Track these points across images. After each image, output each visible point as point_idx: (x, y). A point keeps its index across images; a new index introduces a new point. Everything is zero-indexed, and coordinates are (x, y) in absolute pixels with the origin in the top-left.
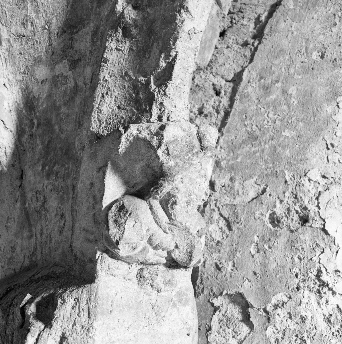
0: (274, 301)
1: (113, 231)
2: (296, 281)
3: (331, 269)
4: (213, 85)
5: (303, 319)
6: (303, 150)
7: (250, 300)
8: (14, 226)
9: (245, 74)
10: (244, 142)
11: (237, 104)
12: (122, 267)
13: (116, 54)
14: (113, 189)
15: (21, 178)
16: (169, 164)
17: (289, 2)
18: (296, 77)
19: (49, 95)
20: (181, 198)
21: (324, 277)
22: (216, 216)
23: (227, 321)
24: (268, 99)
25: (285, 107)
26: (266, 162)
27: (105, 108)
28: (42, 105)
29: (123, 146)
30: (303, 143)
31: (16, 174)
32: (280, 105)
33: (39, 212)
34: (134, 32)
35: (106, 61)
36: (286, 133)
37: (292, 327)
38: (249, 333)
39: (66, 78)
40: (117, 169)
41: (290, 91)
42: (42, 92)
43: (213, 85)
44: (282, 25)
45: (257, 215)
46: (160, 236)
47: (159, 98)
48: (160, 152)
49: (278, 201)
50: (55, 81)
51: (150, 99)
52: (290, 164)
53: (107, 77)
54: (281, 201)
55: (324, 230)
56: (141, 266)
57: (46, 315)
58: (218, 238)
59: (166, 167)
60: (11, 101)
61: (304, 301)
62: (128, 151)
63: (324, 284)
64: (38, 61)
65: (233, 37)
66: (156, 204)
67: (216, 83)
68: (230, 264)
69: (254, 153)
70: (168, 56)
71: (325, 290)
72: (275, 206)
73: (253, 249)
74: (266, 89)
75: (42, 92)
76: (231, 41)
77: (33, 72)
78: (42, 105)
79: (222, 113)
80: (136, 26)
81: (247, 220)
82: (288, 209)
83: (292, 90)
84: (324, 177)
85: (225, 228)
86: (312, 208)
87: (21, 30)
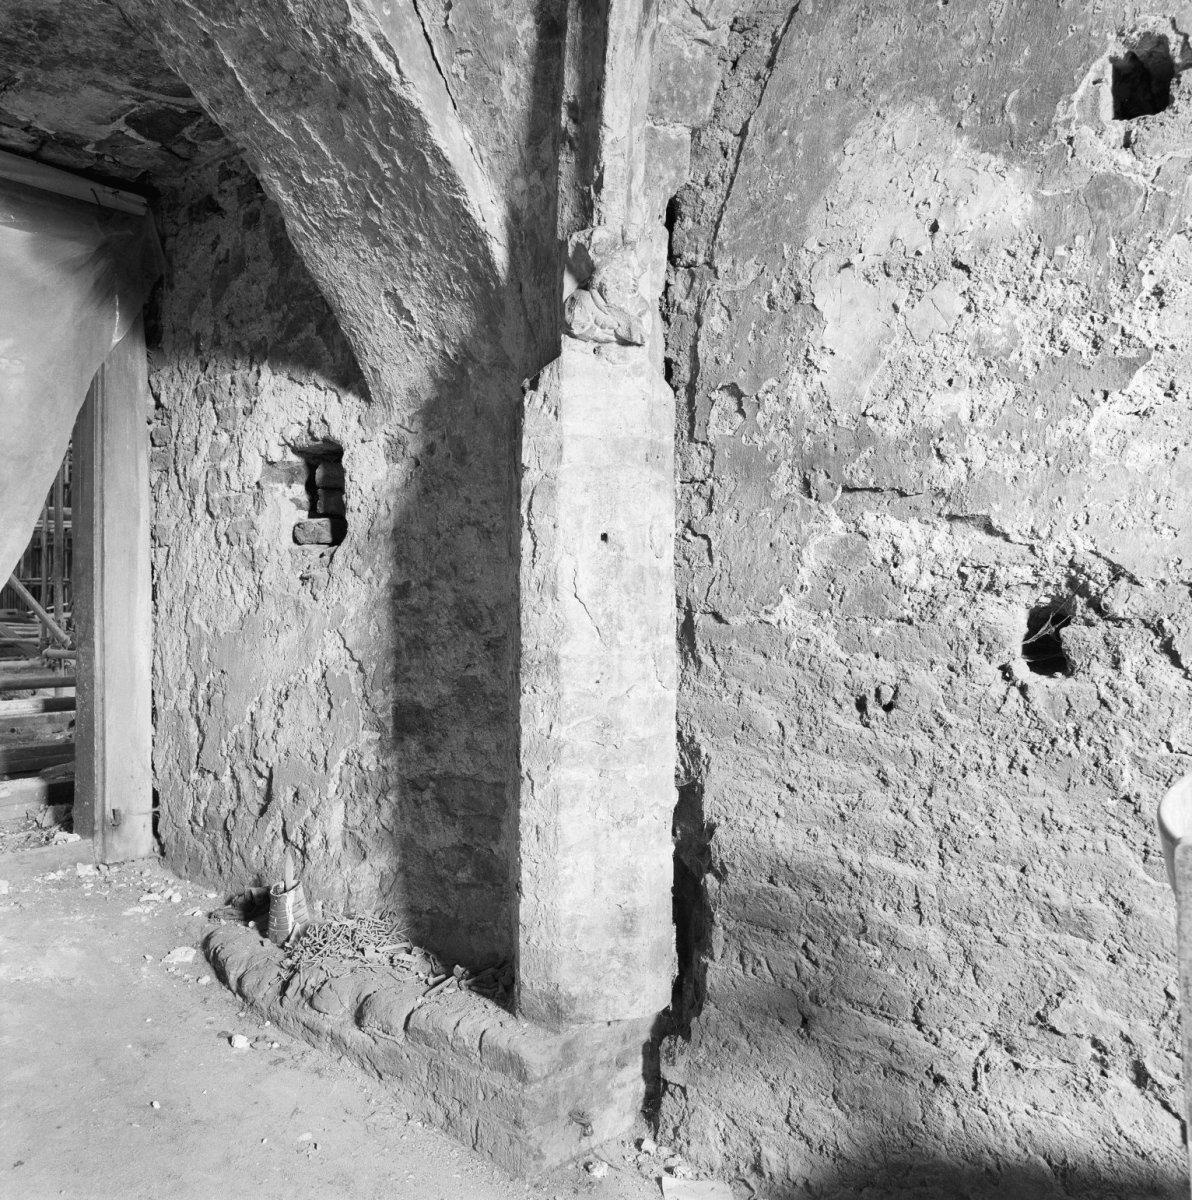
0: (765, 387)
1: (568, 316)
2: (787, 364)
3: (818, 346)
4: (721, 143)
5: (789, 400)
6: (803, 217)
7: (743, 389)
8: (522, 340)
9: (751, 124)
10: (746, 215)
11: (741, 164)
12: (578, 344)
13: (567, 163)
14: (569, 285)
15: (521, 290)
16: (597, 260)
17: (808, 8)
18: (806, 118)
19: (530, 207)
20: (609, 285)
21: (812, 356)
22: (717, 306)
23: (725, 414)
24: (774, 155)
25: (790, 163)
26: (767, 235)
27: (565, 217)
28: (526, 216)
29: (570, 251)
30: (805, 204)
31: (515, 288)
32: (785, 160)
33: (538, 321)
34: (576, 145)
35: (560, 173)
36: (789, 197)
37: (779, 410)
38: (950, 533)
39: (539, 188)
40: (572, 271)
41: (797, 140)
42: (522, 203)
43: (721, 143)
44: (797, 43)
45: (755, 298)
46: (602, 317)
47: (597, 205)
48: (590, 253)
49: (775, 281)
50: (531, 191)
51: (592, 206)
52: (789, 234)
53: (564, 189)
54: (778, 280)
55: (813, 306)
56: (596, 344)
57: (534, 386)
58: (719, 331)
59: (595, 263)
60: (500, 216)
61: (792, 383)
62: (575, 253)
63: (811, 363)
64: (515, 174)
65: (745, 69)
66: (595, 292)
67: (723, 140)
68: (729, 356)
69: (756, 226)
70: (598, 167)
71: (812, 368)
72: (771, 287)
73: (750, 338)
74: (772, 141)
75: (522, 203)
76: (743, 74)
77: (513, 185)
78: (526, 216)
79: (728, 180)
80: (577, 139)
81: (745, 306)
82: (784, 289)
83: (799, 139)
84: (820, 245)
85: (726, 319)
86: (804, 282)
87: (496, 147)
